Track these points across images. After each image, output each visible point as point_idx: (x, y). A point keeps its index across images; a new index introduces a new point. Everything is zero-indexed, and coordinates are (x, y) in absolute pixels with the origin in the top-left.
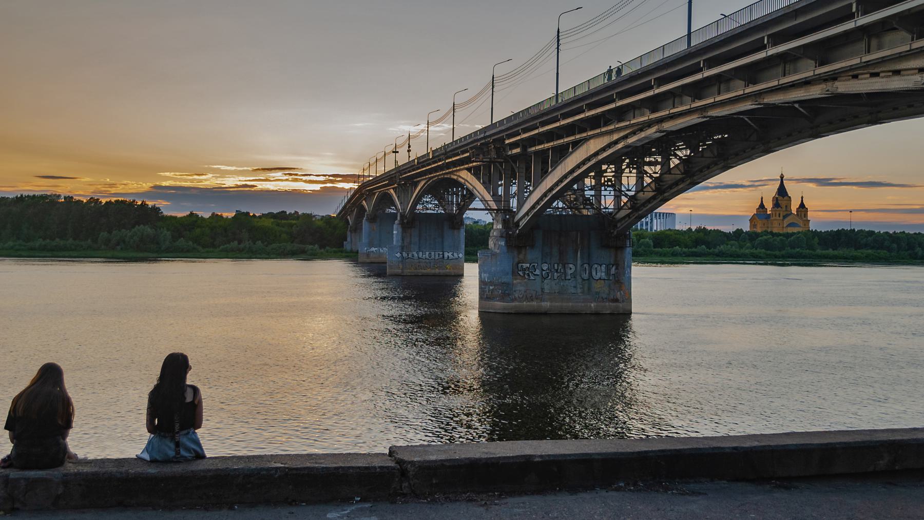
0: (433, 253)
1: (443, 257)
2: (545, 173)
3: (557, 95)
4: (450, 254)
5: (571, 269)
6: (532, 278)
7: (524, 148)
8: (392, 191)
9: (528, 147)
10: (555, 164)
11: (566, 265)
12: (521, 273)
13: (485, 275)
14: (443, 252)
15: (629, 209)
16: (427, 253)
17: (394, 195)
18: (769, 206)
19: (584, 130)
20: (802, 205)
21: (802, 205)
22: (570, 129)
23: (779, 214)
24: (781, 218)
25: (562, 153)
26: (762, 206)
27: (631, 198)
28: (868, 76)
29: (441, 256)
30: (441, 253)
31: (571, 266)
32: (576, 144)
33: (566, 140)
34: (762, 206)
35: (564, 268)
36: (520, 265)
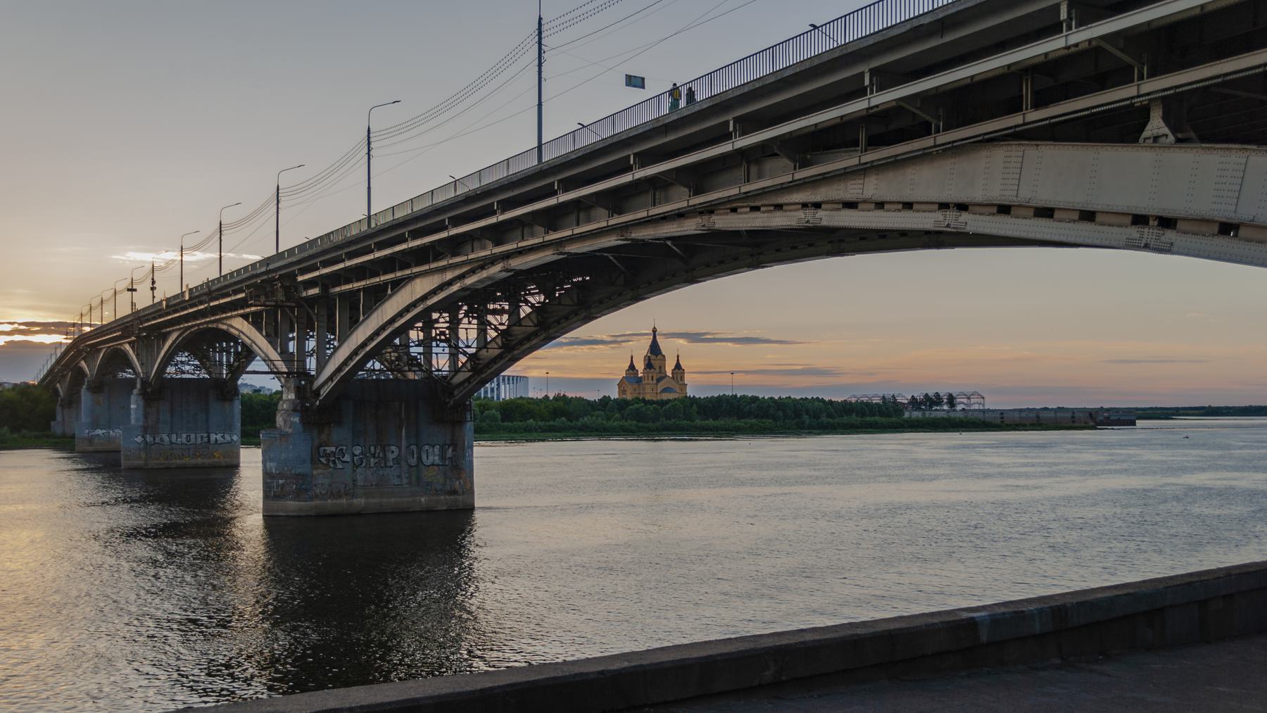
0: (193, 436)
1: (209, 440)
2: (354, 323)
3: (369, 217)
4: (219, 437)
5: (393, 452)
6: (340, 466)
7: (325, 289)
8: (127, 347)
9: (330, 286)
10: (369, 310)
11: (387, 448)
12: (323, 460)
13: (272, 464)
14: (209, 434)
15: (469, 371)
16: (184, 436)
17: (131, 352)
18: (640, 366)
19: (1123, 76)
20: (678, 366)
21: (678, 366)
22: (388, 264)
23: (652, 377)
24: (655, 381)
25: (378, 295)
26: (632, 367)
27: (472, 357)
28: (748, 209)
29: (206, 440)
30: (206, 435)
31: (393, 448)
32: (397, 285)
33: (383, 278)
34: (632, 367)
35: (384, 451)
36: (322, 449)
